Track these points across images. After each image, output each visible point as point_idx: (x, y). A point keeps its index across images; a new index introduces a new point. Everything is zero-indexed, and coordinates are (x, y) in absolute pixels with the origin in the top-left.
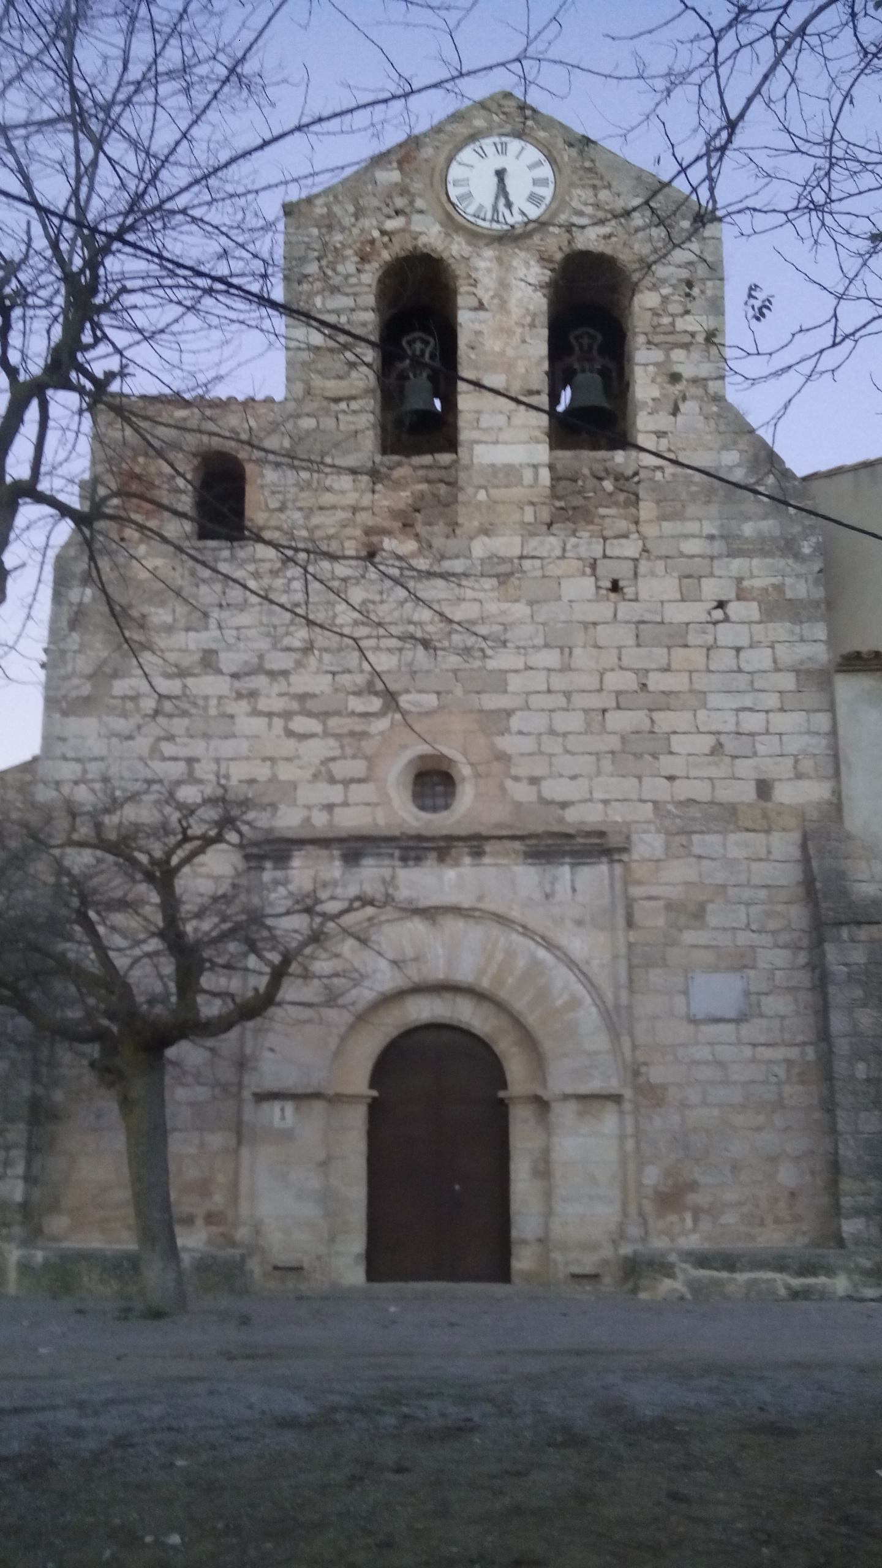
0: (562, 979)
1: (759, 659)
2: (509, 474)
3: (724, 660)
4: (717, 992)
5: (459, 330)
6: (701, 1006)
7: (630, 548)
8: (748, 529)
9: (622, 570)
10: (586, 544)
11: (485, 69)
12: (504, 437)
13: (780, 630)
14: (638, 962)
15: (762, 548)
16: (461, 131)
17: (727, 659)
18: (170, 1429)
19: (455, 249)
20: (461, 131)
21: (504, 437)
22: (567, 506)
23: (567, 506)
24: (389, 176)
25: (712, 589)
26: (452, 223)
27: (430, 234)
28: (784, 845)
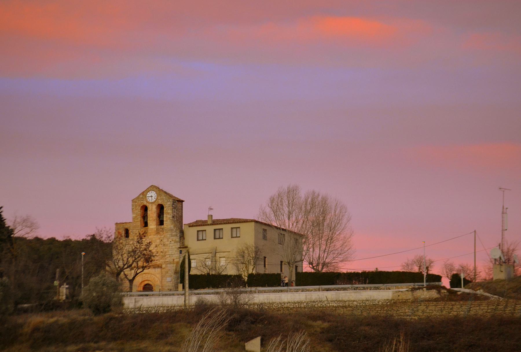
0: (157, 279)
1: (174, 247)
2: (152, 229)
3: (171, 247)
4: (169, 279)
5: (380, 270)
6: (168, 281)
7: (163, 236)
8: (173, 234)
9: (162, 239)
10: (159, 236)
11: (241, 222)
12: (152, 225)
13: (176, 244)
14: (162, 277)
15: (174, 236)
16: (148, 191)
17: (171, 247)
18: (324, 251)
19: (147, 205)
20: (148, 191)
21: (152, 225)
22: (158, 232)
23: (158, 232)
24: (141, 196)
25: (170, 240)
26: (147, 202)
27: (145, 203)
28: (175, 265)
